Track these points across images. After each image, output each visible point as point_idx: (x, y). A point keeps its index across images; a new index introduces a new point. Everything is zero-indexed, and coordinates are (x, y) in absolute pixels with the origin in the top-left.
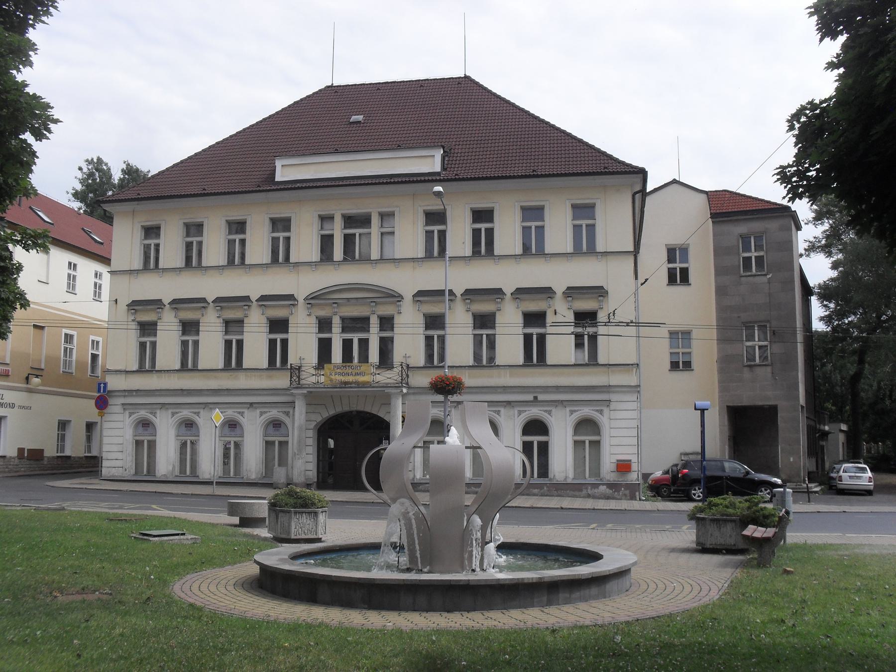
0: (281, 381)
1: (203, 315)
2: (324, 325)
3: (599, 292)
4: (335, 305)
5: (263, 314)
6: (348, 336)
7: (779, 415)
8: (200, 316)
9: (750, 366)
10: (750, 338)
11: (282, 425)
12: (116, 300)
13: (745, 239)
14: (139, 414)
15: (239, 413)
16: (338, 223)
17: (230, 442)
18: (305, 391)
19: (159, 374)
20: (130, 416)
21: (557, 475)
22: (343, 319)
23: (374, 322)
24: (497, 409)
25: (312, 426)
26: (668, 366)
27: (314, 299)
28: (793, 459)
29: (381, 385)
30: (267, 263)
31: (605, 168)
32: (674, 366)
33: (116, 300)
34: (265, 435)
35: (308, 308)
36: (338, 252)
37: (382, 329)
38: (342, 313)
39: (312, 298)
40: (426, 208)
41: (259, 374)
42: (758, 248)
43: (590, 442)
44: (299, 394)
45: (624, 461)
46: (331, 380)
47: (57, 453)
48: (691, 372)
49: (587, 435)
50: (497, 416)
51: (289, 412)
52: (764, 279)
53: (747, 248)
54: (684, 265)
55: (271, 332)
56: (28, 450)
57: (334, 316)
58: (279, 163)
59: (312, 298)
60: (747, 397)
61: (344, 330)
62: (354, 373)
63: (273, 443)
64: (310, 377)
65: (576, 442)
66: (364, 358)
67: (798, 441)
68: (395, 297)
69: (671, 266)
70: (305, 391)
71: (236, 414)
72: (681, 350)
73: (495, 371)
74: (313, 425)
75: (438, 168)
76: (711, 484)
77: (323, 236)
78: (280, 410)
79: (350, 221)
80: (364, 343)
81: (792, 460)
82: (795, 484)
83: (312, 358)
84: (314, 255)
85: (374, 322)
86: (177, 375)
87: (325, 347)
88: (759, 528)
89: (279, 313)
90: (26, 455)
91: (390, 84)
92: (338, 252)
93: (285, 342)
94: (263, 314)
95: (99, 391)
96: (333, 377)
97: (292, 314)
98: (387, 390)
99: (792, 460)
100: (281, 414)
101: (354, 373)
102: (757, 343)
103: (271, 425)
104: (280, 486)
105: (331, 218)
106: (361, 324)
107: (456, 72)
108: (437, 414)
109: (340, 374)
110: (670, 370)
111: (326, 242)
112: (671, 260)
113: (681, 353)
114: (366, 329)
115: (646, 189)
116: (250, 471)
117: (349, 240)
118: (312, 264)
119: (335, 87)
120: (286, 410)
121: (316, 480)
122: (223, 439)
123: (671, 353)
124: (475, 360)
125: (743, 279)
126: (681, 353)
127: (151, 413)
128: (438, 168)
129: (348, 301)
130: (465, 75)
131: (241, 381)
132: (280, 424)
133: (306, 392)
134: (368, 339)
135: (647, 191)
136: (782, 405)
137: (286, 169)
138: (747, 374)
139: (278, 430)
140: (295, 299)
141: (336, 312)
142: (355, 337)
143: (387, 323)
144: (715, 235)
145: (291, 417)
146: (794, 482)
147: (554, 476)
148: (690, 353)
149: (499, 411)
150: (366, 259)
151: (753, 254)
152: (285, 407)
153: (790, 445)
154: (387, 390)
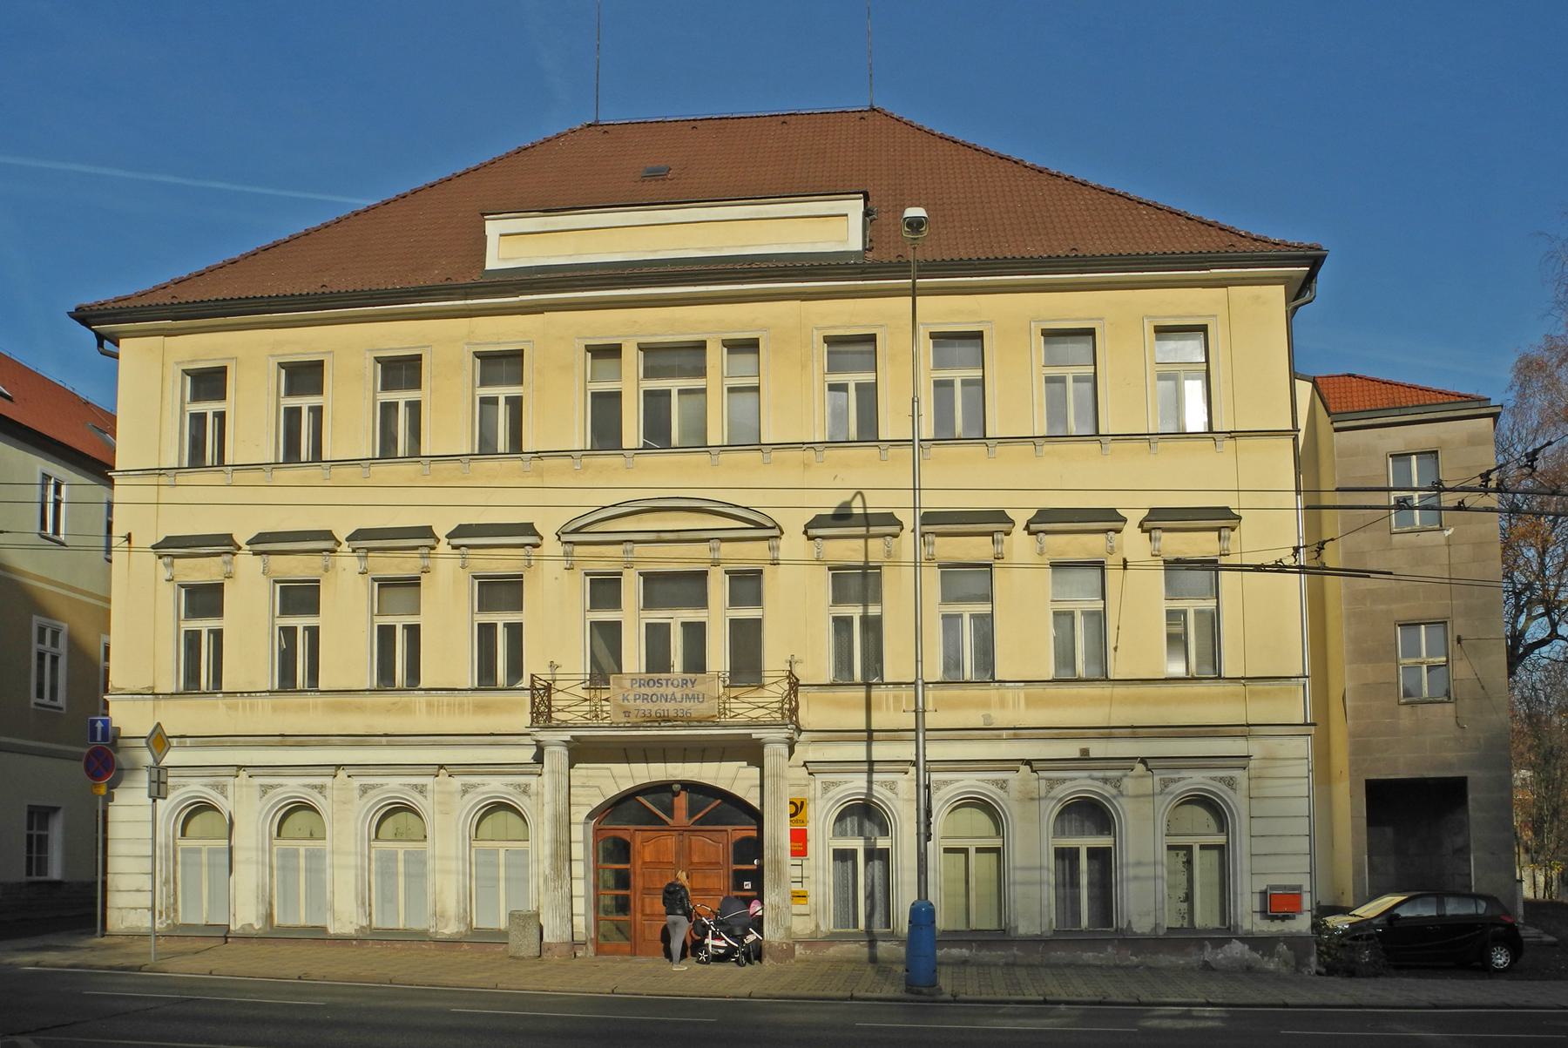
0: (515, 713)
2: (605, 590)
3: (1222, 518)
6: (658, 616)
7: (1470, 797)
8: (321, 571)
12: (129, 535)
16: (632, 360)
19: (230, 700)
21: (1134, 919)
22: (649, 578)
23: (718, 588)
27: (574, 534)
33: (129, 535)
36: (632, 428)
37: (735, 601)
39: (576, 531)
45: (1285, 887)
47: (29, 873)
49: (1082, 833)
55: (484, 606)
56: (736, 862)
58: (493, 228)
59: (576, 531)
61: (649, 603)
62: (678, 696)
64: (571, 702)
66: (695, 661)
68: (764, 529)
75: (856, 244)
76: (1457, 938)
77: (596, 396)
79: (660, 358)
80: (696, 633)
83: (575, 661)
84: (578, 434)
85: (718, 588)
86: (269, 701)
87: (607, 636)
88: (456, 930)
89: (500, 563)
90: (737, 945)
92: (632, 428)
93: (515, 631)
95: (93, 737)
98: (756, 734)
100: (511, 789)
105: (613, 351)
106: (689, 587)
107: (164, 537)
109: (645, 698)
111: (606, 408)
114: (701, 602)
116: (442, 916)
117: (656, 404)
124: (946, 669)
127: (215, 787)
128: (856, 244)
131: (417, 713)
133: (568, 738)
140: (536, 534)
142: (677, 618)
143: (747, 584)
147: (1129, 922)
150: (698, 442)
153: (1493, 854)
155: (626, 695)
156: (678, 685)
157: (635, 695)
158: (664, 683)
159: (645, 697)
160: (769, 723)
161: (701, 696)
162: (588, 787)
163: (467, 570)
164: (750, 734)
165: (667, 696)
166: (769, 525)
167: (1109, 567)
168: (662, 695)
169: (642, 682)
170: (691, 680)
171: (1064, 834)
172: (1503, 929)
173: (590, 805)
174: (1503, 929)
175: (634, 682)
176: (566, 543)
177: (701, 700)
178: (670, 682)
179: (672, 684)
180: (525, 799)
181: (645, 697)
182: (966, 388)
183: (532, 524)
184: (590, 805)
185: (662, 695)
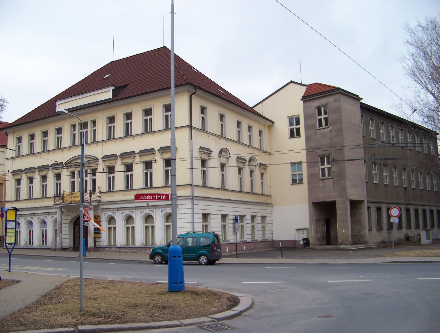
1: (34, 175)
7: (337, 206)
9: (322, 180)
10: (323, 164)
12: (8, 171)
13: (319, 109)
14: (108, 213)
15: (151, 211)
17: (44, 230)
18: (58, 206)
20: (162, 212)
24: (32, 217)
25: (68, 222)
26: (291, 182)
28: (345, 231)
31: (146, 91)
32: (294, 182)
40: (108, 116)
42: (326, 113)
48: (302, 184)
50: (152, 213)
52: (328, 130)
53: (320, 114)
54: (298, 127)
57: (75, 171)
60: (323, 197)
67: (347, 221)
69: (291, 127)
70: (58, 206)
71: (112, 214)
72: (297, 173)
73: (46, 200)
74: (69, 222)
81: (344, 231)
82: (345, 245)
91: (138, 55)
97: (62, 171)
99: (344, 231)
102: (326, 166)
110: (291, 184)
112: (291, 124)
113: (297, 175)
115: (56, 111)
119: (114, 61)
121: (73, 246)
122: (42, 229)
123: (293, 175)
125: (318, 131)
126: (297, 175)
130: (164, 46)
133: (59, 207)
134: (87, 180)
135: (57, 111)
136: (339, 201)
137: (60, 106)
138: (321, 184)
144: (304, 108)
145: (155, 213)
146: (345, 245)
148: (302, 174)
149: (133, 212)
151: (323, 117)
153: (342, 223)
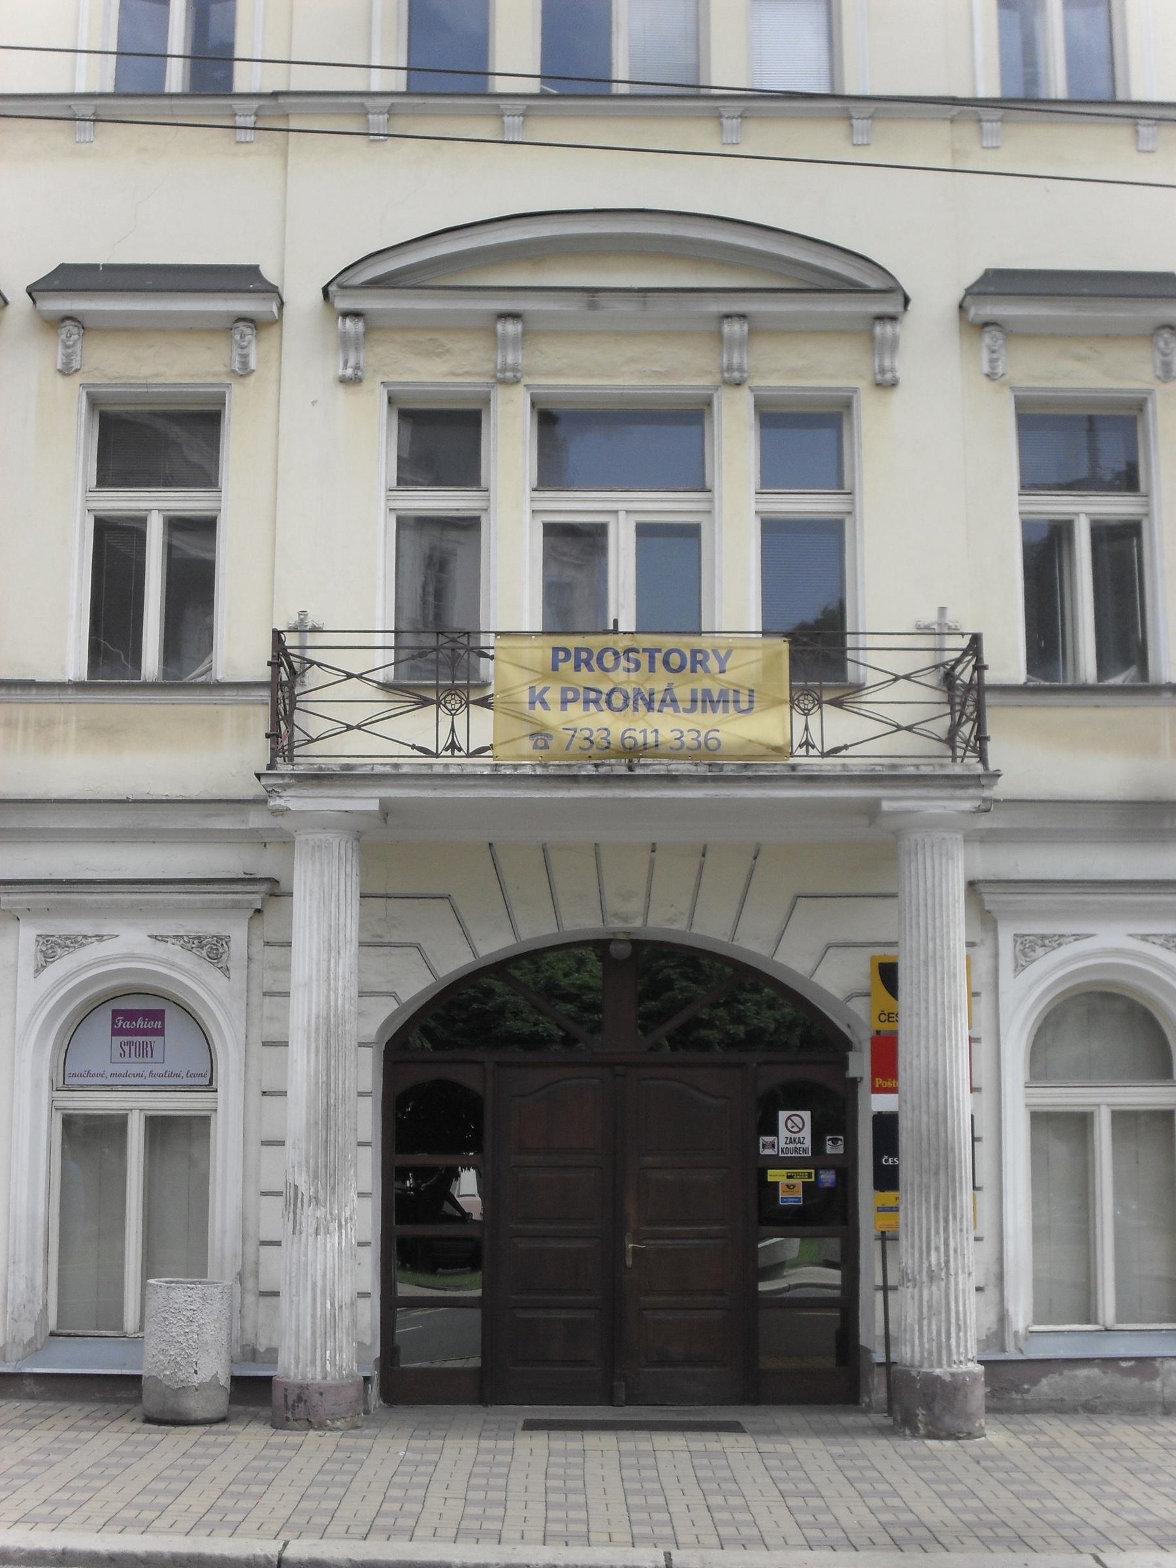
4: (512, 328)
5: (66, 371)
11: (172, 1020)
18: (366, 801)
29: (857, 766)
30: (97, 89)
34: (64, 1081)
35: (346, 343)
38: (548, 374)
41: (33, 711)
43: (1123, 1119)
44: (323, 822)
46: (540, 735)
51: (222, 941)
62: (682, 693)
63: (1081, 1122)
65: (1041, 1120)
70: (366, 801)
78: (168, 927)
94: (66, 371)
96: (553, 717)
97: (245, 372)
100: (173, 951)
101: (682, 693)
103: (104, 1020)
104: (196, 1406)
108: (1118, 952)
118: (368, 102)
120: (209, 927)
129: (593, 306)
132: (159, 1015)
139: (144, 1052)
141: (515, 369)
152: (208, 909)
154: (892, 801)
155: (538, 691)
156: (682, 667)
157: (564, 691)
158: (644, 659)
159: (593, 695)
160: (911, 771)
161: (744, 698)
162: (390, 945)
163: (77, 379)
164: (877, 801)
165: (651, 694)
166: (873, 284)
167: (870, 641)
168: (638, 692)
169: (584, 655)
170: (715, 651)
171: (1026, 1097)
172: (459, 1215)
173: (393, 995)
174: (459, 1215)
175: (561, 655)
176: (346, 314)
177: (744, 706)
178: (659, 657)
179: (666, 663)
180: (212, 976)
181: (593, 695)
182: (211, 559)
183: (257, 266)
184: (393, 995)
185: (638, 692)
